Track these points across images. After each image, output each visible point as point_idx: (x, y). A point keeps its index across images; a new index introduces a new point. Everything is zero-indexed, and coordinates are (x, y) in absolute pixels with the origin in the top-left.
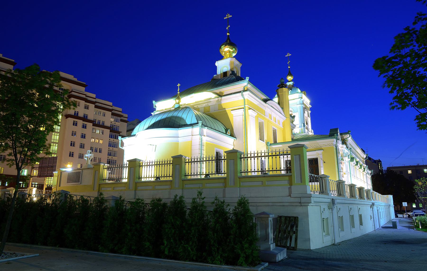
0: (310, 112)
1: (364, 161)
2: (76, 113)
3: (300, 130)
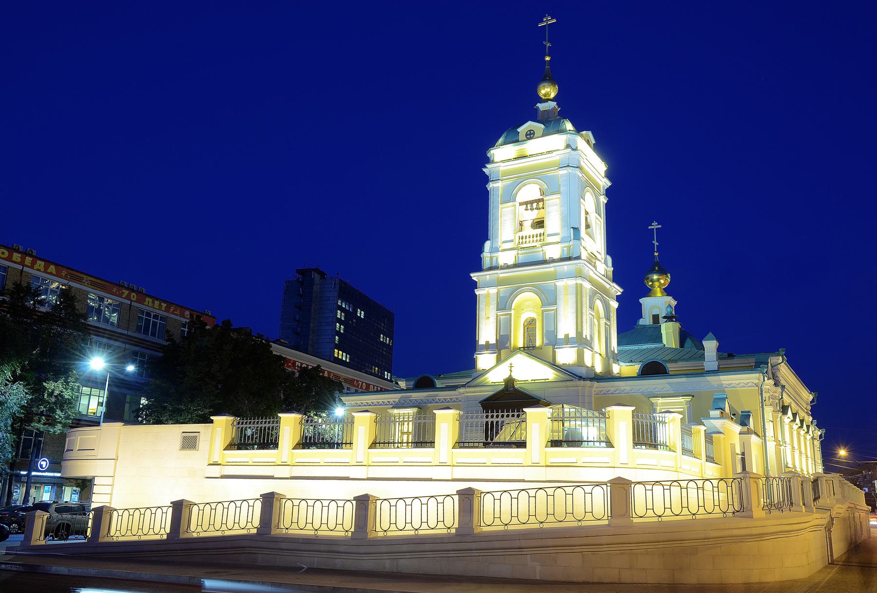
0: (606, 202)
1: (809, 408)
2: (151, 322)
3: (563, 250)
